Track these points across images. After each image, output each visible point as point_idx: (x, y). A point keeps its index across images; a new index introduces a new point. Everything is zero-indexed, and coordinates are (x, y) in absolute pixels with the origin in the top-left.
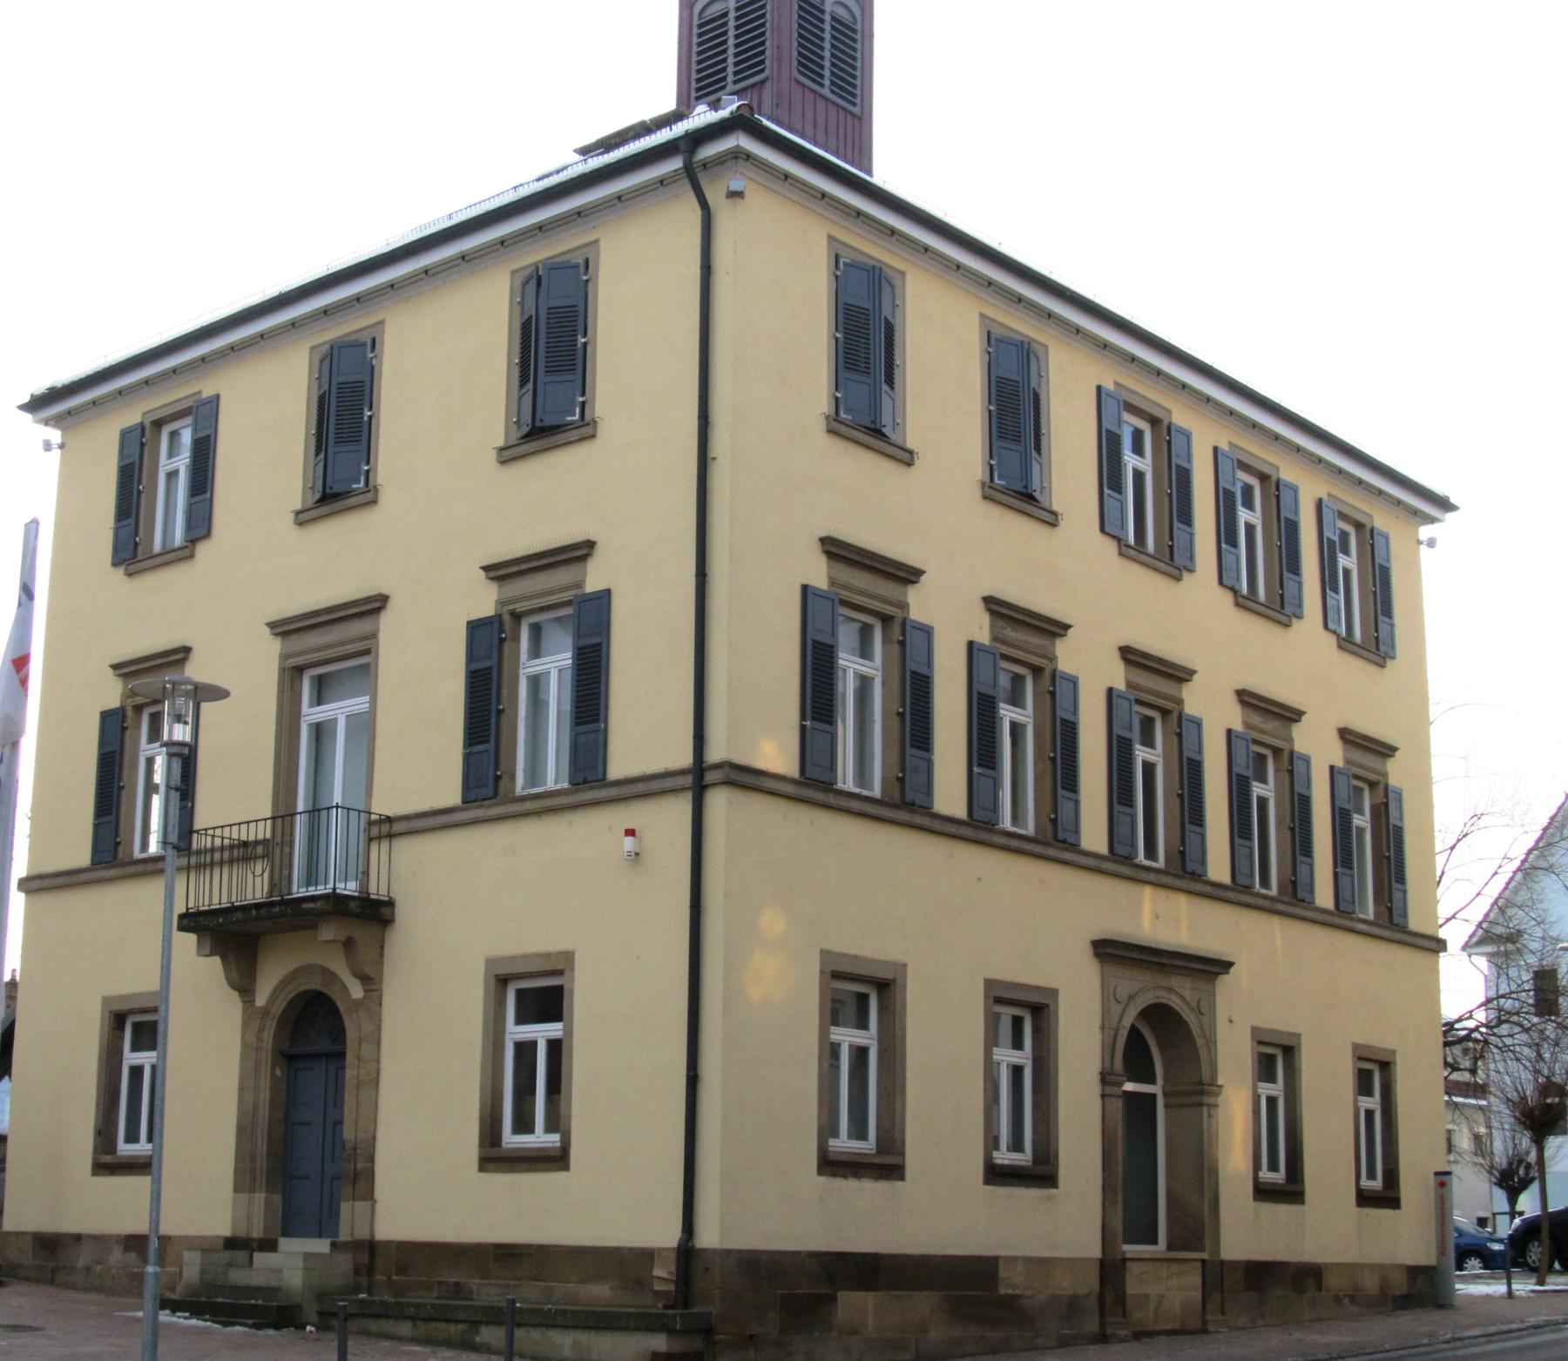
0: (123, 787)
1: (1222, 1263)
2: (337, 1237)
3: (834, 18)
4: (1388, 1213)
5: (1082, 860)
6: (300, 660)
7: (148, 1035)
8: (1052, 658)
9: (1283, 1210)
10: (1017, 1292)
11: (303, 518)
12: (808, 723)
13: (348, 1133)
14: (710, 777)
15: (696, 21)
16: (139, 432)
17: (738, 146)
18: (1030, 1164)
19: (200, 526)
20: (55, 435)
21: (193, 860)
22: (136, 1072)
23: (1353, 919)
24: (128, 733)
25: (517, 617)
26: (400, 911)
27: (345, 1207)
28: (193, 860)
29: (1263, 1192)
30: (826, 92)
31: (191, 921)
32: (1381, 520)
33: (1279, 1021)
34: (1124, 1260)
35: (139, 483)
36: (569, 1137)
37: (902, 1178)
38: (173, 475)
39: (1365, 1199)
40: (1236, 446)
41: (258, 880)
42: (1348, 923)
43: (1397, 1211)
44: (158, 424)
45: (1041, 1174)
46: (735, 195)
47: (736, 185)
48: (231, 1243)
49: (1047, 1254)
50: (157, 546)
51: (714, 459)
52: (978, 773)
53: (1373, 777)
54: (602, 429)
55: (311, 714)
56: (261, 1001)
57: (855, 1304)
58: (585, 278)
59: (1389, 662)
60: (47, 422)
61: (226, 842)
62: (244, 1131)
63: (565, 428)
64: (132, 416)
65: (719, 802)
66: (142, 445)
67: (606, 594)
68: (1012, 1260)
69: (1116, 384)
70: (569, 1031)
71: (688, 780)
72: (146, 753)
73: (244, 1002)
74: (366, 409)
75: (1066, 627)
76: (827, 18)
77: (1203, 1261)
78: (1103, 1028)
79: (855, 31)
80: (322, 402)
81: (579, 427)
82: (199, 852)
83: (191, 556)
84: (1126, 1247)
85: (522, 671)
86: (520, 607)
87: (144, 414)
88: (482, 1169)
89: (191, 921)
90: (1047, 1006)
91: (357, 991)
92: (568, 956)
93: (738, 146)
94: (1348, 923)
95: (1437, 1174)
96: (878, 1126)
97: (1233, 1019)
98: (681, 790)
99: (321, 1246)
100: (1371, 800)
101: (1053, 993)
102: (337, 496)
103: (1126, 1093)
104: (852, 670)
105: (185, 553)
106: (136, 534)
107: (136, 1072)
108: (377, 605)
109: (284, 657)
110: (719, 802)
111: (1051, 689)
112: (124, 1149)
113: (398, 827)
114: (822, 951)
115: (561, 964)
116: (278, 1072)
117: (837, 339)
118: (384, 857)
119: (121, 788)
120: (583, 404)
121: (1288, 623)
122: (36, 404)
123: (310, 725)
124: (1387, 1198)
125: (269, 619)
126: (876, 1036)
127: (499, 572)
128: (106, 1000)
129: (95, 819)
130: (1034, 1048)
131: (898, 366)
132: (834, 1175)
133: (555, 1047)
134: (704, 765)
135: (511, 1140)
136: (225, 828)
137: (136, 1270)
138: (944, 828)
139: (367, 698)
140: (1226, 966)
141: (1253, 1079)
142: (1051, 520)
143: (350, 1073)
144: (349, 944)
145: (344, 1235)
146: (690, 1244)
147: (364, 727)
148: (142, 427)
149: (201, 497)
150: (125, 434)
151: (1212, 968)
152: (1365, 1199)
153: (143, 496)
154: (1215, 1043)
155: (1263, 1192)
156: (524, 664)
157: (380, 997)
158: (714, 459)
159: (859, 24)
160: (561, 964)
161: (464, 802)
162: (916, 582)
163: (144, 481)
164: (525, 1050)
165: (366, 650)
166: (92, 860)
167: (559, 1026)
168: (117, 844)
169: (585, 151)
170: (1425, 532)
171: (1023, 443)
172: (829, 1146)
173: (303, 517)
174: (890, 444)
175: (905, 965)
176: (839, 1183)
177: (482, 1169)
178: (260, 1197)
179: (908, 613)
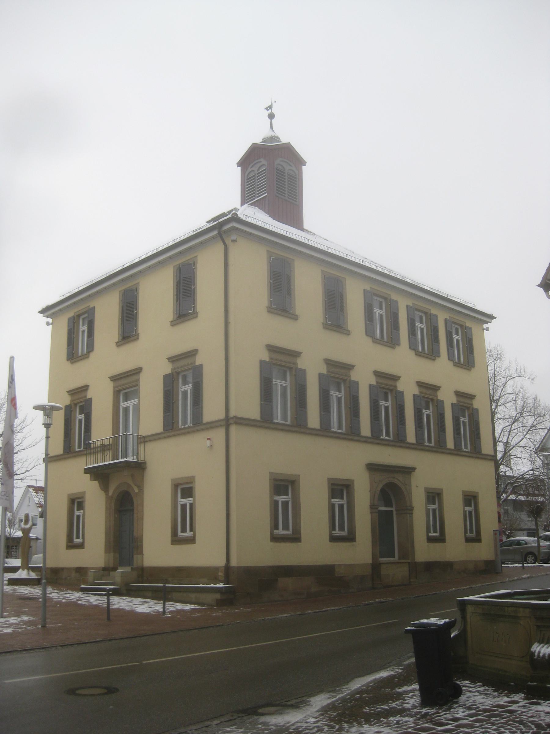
0: (72, 429)
1: (416, 563)
2: (133, 566)
3: (288, 175)
4: (477, 544)
5: (362, 439)
6: (119, 388)
7: (81, 506)
8: (350, 376)
9: (438, 545)
10: (342, 575)
11: (118, 344)
12: (263, 403)
13: (135, 534)
14: (230, 421)
15: (246, 178)
16: (73, 319)
17: (233, 226)
18: (347, 535)
19: (91, 347)
20: (50, 320)
21: (92, 451)
22: (78, 517)
23: (461, 451)
24: (73, 412)
25: (178, 373)
26: (148, 465)
27: (135, 556)
28: (92, 451)
29: (430, 540)
30: (286, 198)
31: (87, 471)
32: (468, 324)
33: (435, 484)
34: (380, 564)
35: (74, 335)
36: (195, 534)
37: (300, 541)
38: (83, 331)
39: (468, 540)
40: (414, 304)
41: (106, 457)
42: (459, 453)
43: (481, 543)
44: (79, 316)
45: (350, 538)
46: (234, 241)
47: (234, 237)
48: (105, 569)
49: (353, 563)
50: (80, 354)
51: (230, 323)
52: (323, 414)
53: (468, 405)
54: (199, 315)
55: (123, 405)
56: (110, 494)
57: (285, 582)
58: (194, 268)
59: (472, 369)
60: (47, 317)
61: (99, 445)
62: (107, 534)
63: (189, 314)
64: (71, 314)
65: (233, 429)
66: (74, 323)
67: (201, 365)
68: (340, 565)
69: (450, 317)
70: (194, 500)
71: (224, 423)
72: (78, 418)
73: (106, 495)
74: (135, 310)
75: (354, 366)
76: (286, 175)
77: (409, 563)
78: (370, 491)
79: (296, 178)
80: (123, 307)
81: (193, 314)
82: (94, 448)
83: (88, 357)
84: (381, 559)
85: (180, 390)
86: (178, 370)
87: (75, 313)
88: (172, 544)
89: (87, 471)
90: (350, 485)
91: (136, 490)
92: (193, 478)
93: (233, 226)
94: (459, 453)
95: (494, 531)
96: (292, 525)
97: (417, 485)
98: (221, 426)
99: (127, 570)
100: (468, 413)
101: (353, 481)
102: (129, 337)
103: (379, 510)
104: (279, 385)
105: (86, 356)
106: (73, 351)
107: (78, 517)
108: (139, 371)
109: (114, 388)
110: (233, 429)
111: (349, 386)
112: (76, 541)
113: (147, 439)
114: (270, 472)
115: (191, 480)
116: (116, 516)
117: (271, 282)
118: (142, 449)
119: (71, 429)
120: (194, 307)
121: (435, 359)
122: (43, 312)
123: (123, 408)
124: (478, 539)
125: (110, 376)
126: (291, 498)
127: (172, 359)
128: (69, 495)
129: (164, 414)
130: (347, 498)
131: (292, 289)
132: (276, 542)
133: (191, 505)
134: (229, 418)
135: (180, 534)
136: (101, 441)
137: (79, 578)
138: (313, 433)
139: (137, 399)
140: (414, 469)
141: (271, 527)
142: (348, 333)
143: (135, 515)
144: (132, 476)
145: (135, 565)
146: (228, 565)
147: (137, 408)
148: (74, 317)
149: (91, 338)
150: (69, 319)
151: (408, 471)
152: (468, 540)
153: (75, 339)
154: (411, 493)
155: (430, 540)
156: (180, 388)
157: (143, 491)
158: (230, 323)
159: (297, 176)
160: (191, 480)
161: (164, 431)
162: (300, 356)
163: (75, 334)
164: (184, 506)
165: (137, 384)
166: (64, 452)
167: (191, 499)
168: (70, 447)
169: (208, 222)
170: (485, 326)
171: (336, 310)
172: (274, 533)
173: (118, 344)
174: (290, 314)
175: (299, 475)
176: (278, 544)
177: (172, 544)
178: (112, 554)
179: (297, 366)
